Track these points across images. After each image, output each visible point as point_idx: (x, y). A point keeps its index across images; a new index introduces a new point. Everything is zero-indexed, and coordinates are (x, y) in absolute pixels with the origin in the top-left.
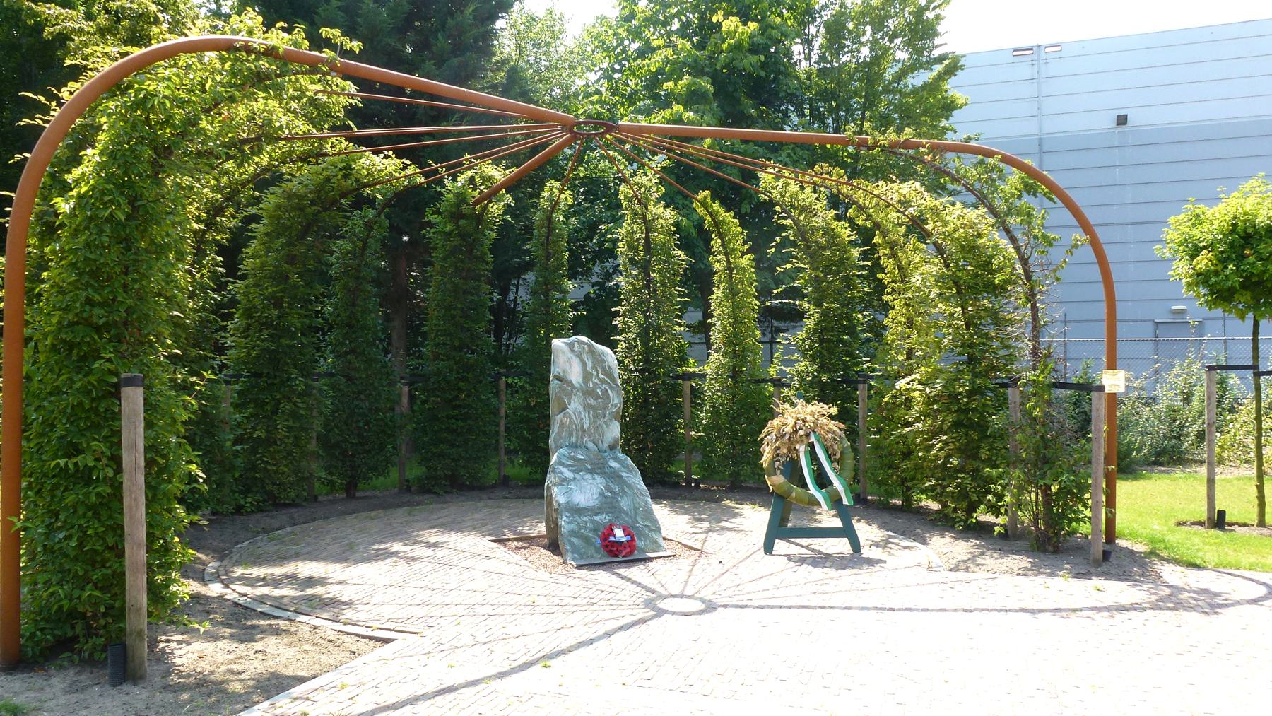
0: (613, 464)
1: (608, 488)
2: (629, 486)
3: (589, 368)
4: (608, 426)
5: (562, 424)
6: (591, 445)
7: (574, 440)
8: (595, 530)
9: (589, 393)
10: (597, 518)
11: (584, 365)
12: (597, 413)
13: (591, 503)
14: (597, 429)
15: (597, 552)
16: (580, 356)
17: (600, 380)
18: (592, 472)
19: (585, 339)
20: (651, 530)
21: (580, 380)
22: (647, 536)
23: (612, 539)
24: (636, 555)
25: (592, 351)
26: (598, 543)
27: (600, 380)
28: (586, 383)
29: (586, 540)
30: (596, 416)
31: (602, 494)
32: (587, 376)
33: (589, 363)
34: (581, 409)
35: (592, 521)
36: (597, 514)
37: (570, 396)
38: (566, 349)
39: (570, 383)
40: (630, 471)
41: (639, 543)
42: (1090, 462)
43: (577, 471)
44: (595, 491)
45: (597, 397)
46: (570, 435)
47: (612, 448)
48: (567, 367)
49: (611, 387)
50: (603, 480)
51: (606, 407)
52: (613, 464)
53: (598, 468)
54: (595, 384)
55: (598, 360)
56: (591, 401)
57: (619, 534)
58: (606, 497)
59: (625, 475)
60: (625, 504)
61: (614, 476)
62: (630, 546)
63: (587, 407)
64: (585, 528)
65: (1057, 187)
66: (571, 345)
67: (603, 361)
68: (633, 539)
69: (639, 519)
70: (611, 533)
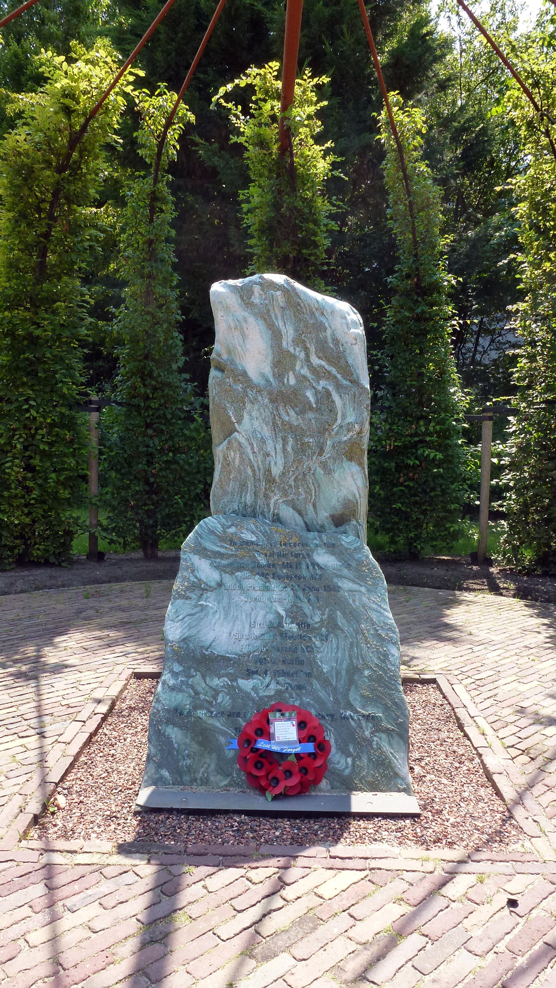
0: (324, 559)
1: (295, 613)
2: (353, 616)
3: (287, 343)
4: (329, 472)
5: (227, 463)
6: (287, 512)
7: (249, 499)
8: (232, 715)
9: (284, 398)
10: (246, 684)
11: (276, 336)
12: (303, 445)
13: (243, 647)
14: (301, 479)
15: (222, 771)
16: (265, 316)
17: (313, 370)
18: (266, 573)
19: (279, 278)
20: (378, 729)
21: (267, 370)
22: (365, 745)
23: (262, 744)
24: (320, 799)
25: (293, 302)
26: (231, 748)
27: (313, 370)
28: (280, 376)
29: (203, 736)
30: (302, 449)
31: (276, 627)
32: (281, 361)
33: (288, 332)
34: (266, 432)
35: (232, 690)
36: (249, 674)
37: (240, 403)
38: (233, 301)
39: (242, 376)
40: (361, 577)
41: (338, 760)
42: (176, 710)
43: (233, 568)
44: (262, 617)
45: (304, 408)
46: (243, 486)
47: (340, 521)
48: (236, 339)
49: (338, 386)
50: (287, 595)
51: (324, 430)
52: (324, 559)
53: (286, 565)
54: (301, 379)
55: (311, 324)
56: (291, 416)
57: (285, 733)
58: (284, 635)
59: (346, 585)
60: (328, 656)
61: (320, 587)
62: (308, 770)
63: (281, 429)
64: (208, 705)
65: (382, 962)
66: (244, 294)
67: (320, 327)
68: (322, 748)
69: (354, 697)
70: (264, 731)
